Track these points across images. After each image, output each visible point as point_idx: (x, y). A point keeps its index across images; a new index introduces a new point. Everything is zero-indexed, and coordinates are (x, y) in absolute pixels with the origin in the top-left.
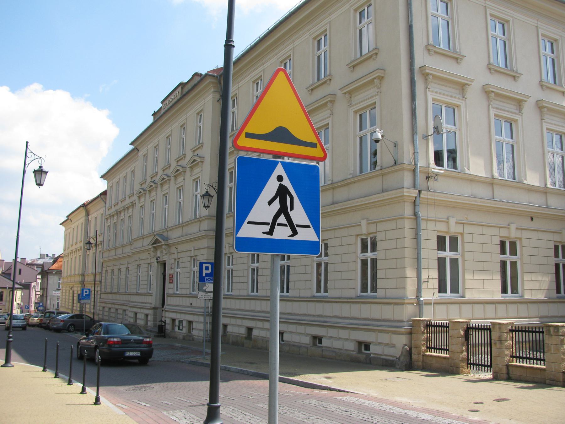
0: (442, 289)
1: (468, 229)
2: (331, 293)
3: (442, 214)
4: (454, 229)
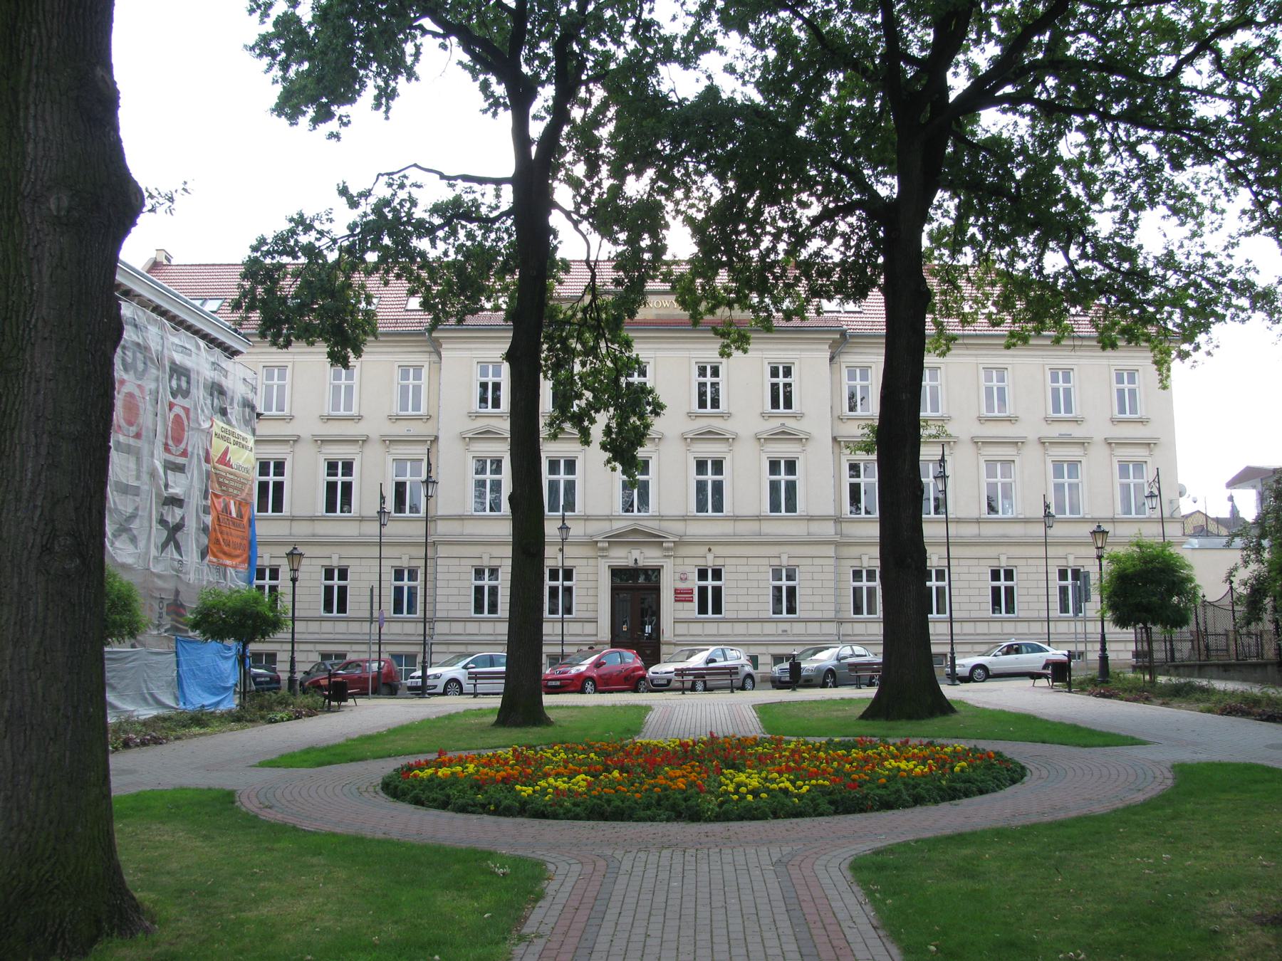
0: (858, 610)
1: (728, 561)
4: (1004, 563)
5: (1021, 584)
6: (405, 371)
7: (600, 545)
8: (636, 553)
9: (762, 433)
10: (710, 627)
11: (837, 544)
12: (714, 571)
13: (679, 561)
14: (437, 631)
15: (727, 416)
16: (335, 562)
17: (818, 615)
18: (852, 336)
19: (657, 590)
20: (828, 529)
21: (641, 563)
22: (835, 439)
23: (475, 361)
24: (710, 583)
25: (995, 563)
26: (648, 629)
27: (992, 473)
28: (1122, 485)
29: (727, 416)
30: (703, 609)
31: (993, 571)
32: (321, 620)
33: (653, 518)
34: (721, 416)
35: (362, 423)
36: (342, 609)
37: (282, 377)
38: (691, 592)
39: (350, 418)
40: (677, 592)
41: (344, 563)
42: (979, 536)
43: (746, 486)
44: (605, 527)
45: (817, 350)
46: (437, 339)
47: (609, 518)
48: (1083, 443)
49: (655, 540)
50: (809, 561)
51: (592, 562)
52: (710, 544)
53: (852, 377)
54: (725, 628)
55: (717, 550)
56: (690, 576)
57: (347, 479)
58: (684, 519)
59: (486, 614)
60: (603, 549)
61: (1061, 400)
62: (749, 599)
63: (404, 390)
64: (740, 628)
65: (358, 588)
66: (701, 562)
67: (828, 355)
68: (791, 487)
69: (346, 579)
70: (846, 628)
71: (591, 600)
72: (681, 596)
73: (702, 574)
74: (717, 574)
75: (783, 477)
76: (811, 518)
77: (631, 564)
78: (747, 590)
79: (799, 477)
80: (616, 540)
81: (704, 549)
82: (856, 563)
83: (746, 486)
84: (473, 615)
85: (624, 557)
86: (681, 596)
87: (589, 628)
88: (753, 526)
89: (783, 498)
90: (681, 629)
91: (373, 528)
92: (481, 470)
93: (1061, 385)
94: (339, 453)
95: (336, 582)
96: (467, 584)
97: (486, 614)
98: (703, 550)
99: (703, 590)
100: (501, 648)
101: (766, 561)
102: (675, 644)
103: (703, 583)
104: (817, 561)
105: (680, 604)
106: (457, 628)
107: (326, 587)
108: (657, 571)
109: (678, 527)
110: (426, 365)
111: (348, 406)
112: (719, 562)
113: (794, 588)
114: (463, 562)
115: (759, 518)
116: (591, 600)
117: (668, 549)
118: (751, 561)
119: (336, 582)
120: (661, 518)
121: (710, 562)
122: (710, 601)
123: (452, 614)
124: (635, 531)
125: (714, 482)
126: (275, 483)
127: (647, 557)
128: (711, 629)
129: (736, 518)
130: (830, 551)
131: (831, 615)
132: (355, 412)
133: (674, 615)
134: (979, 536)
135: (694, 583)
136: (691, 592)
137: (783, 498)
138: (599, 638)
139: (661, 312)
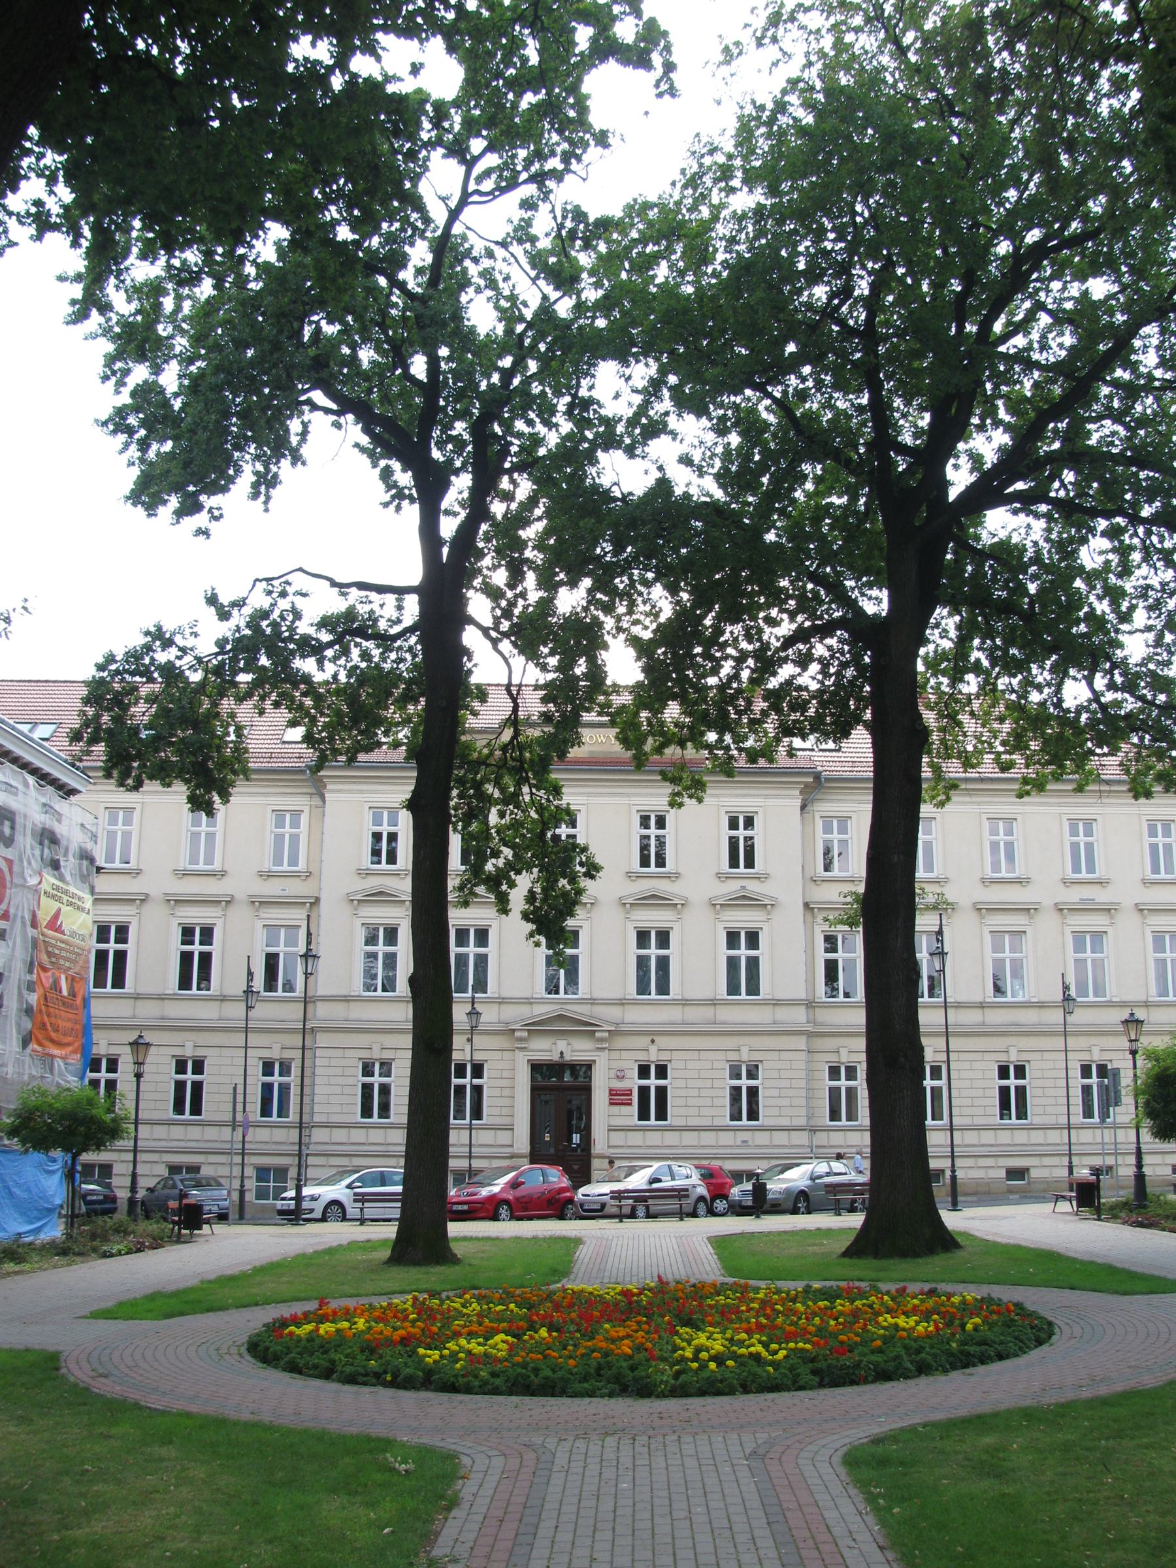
0: (835, 1115)
1: (676, 1055)
5: (1035, 1083)
6: (279, 815)
7: (517, 1034)
8: (562, 1045)
10: (653, 1137)
11: (810, 1035)
12: (657, 1067)
13: (615, 1055)
15: (675, 876)
16: (189, 1052)
17: (785, 1122)
18: (828, 780)
19: (586, 1090)
20: (798, 1017)
21: (568, 1057)
22: (806, 905)
23: (984, 817)
24: (653, 1082)
25: (1003, 1057)
26: (576, 1138)
27: (998, 948)
28: (1157, 960)
29: (675, 876)
30: (644, 1115)
33: (582, 1001)
35: (226, 880)
37: (128, 821)
38: (629, 1093)
39: (211, 874)
41: (200, 1052)
42: (984, 1024)
43: (698, 963)
44: (524, 1012)
47: (529, 1001)
48: (1108, 910)
49: (585, 1028)
51: (507, 1055)
52: (653, 1035)
53: (828, 829)
54: (671, 1138)
55: (662, 1041)
56: (628, 1074)
58: (622, 1002)
59: (275, 1118)
60: (521, 1039)
61: (1083, 857)
62: (701, 1102)
64: (690, 1138)
66: (642, 1056)
67: (798, 802)
68: (663, 963)
69: (665, 1078)
70: (821, 1138)
71: (506, 1102)
72: (618, 1098)
73: (644, 1072)
74: (662, 1072)
75: (653, 952)
76: (777, 1003)
77: (555, 1057)
78: (699, 1092)
80: (537, 1028)
82: (833, 1058)
83: (698, 963)
85: (548, 1049)
86: (618, 1098)
87: (503, 1137)
88: (706, 1013)
89: (744, 977)
90: (617, 1138)
91: (238, 1010)
92: (371, 940)
94: (197, 916)
96: (351, 1081)
97: (275, 1118)
99: (644, 1091)
101: (720, 1056)
104: (784, 1055)
106: (340, 1135)
107: (365, 1086)
108: (589, 1066)
109: (614, 1013)
110: (306, 809)
112: (664, 1056)
113: (1024, 1088)
114: (348, 1053)
115: (713, 1002)
116: (506, 1102)
117: (602, 1040)
118: (704, 1055)
120: (593, 1002)
121: (653, 1056)
122: (653, 1105)
124: (561, 1018)
127: (575, 1050)
128: (654, 1138)
129: (685, 1002)
130: (801, 1043)
131: (802, 1122)
132: (217, 866)
133: (608, 1123)
134: (984, 1024)
135: (634, 1082)
136: (629, 1093)
137: (744, 977)
138: (516, 1150)
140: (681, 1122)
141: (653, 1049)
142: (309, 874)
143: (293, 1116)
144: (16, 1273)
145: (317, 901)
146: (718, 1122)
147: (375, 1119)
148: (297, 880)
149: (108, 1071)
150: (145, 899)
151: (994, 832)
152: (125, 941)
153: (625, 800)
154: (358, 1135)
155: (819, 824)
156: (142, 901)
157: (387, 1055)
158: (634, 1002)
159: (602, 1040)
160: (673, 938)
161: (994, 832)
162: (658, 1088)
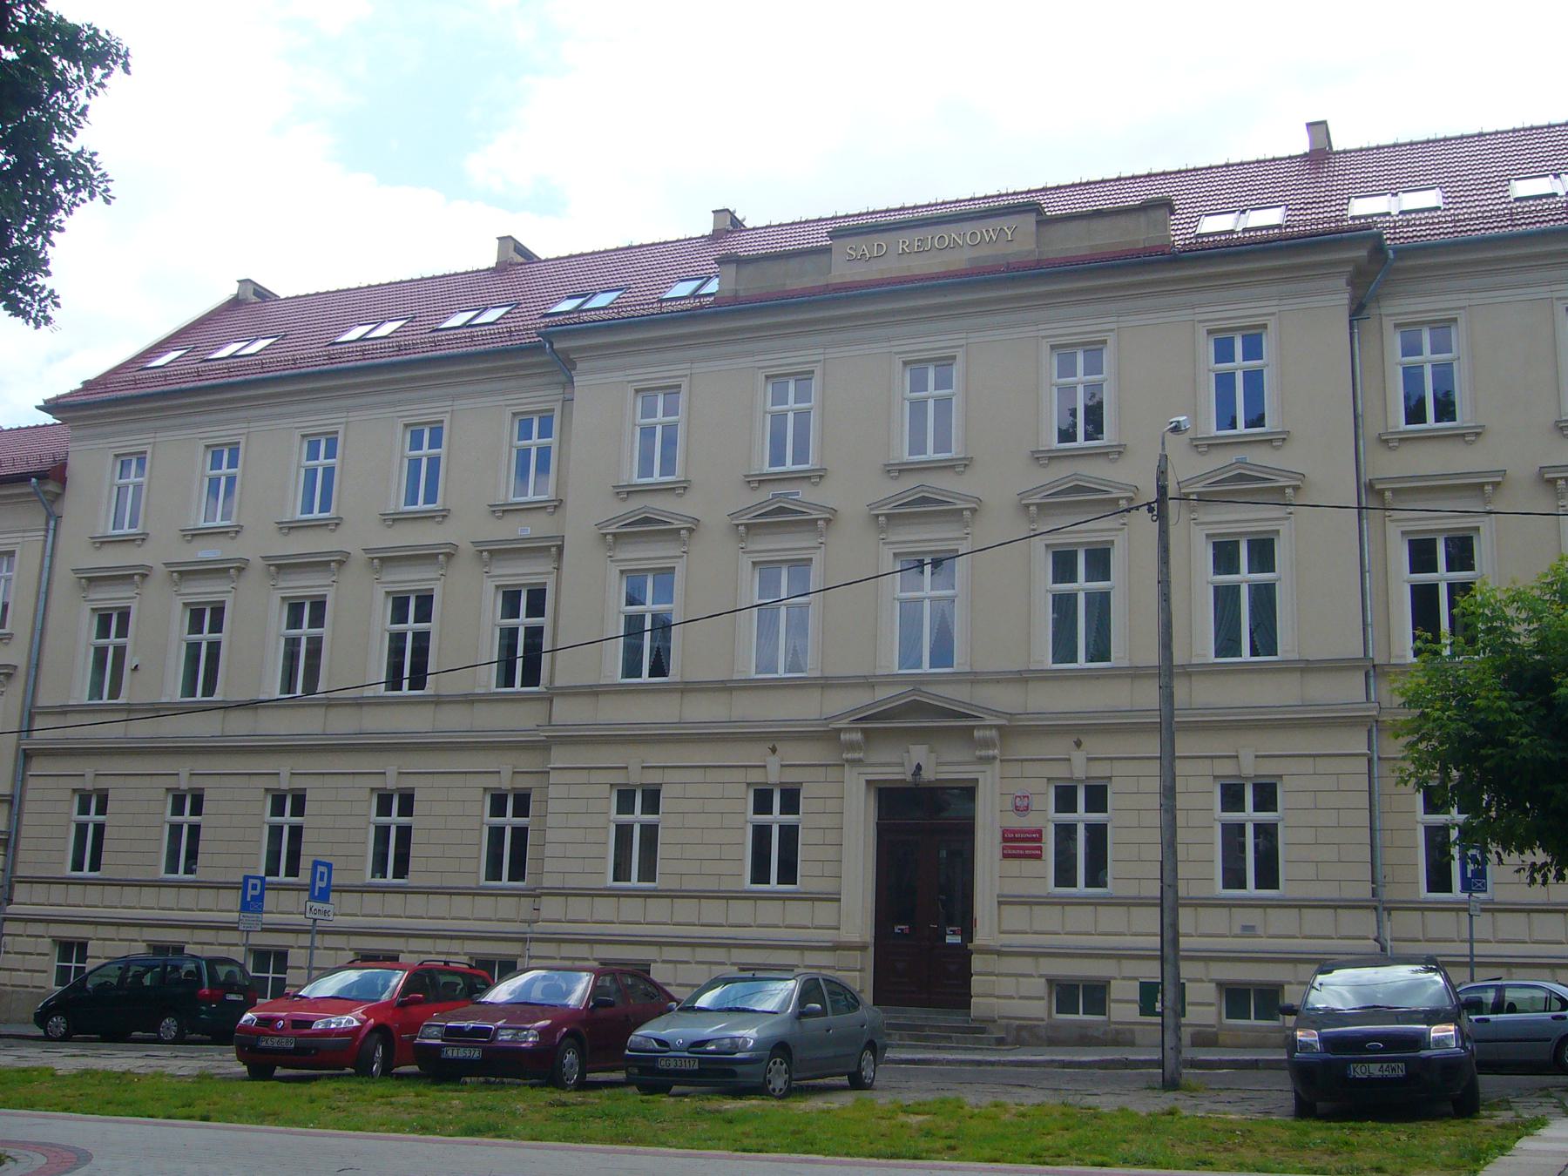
2: (201, 874)
3: (753, 754)
4: (1250, 768)
8: (918, 753)
9: (610, 522)
14: (544, 914)
19: (966, 831)
21: (928, 775)
24: (1081, 816)
29: (1276, 441)
30: (1065, 875)
31: (1226, 789)
32: (1423, 908)
34: (1103, 454)
36: (1096, 875)
38: (1037, 836)
40: (1009, 836)
45: (281, 416)
46: (566, 351)
47: (869, 682)
50: (1308, 766)
51: (833, 773)
52: (1077, 730)
56: (1035, 803)
57: (422, 626)
58: (1024, 678)
59: (634, 882)
60: (852, 746)
61: (1243, 404)
63: (1225, 383)
65: (1131, 825)
66: (1060, 771)
70: (1403, 924)
73: (1065, 799)
79: (1282, 575)
80: (881, 725)
81: (764, 748)
84: (483, 882)
86: (1020, 845)
87: (824, 912)
90: (1016, 917)
93: (1239, 365)
95: (776, 818)
98: (1059, 747)
99: (1065, 833)
100: (855, 958)
101: (739, 775)
102: (999, 953)
103: (1066, 817)
105: (1014, 866)
106: (579, 907)
107: (619, 828)
108: (968, 792)
111: (943, 443)
112: (1099, 770)
114: (597, 776)
119: (776, 818)
120: (974, 678)
121: (1080, 769)
123: (449, 881)
125: (310, 640)
126: (1089, 596)
127: (938, 764)
129: (1307, 667)
132: (956, 452)
135: (1046, 817)
139: (984, 251)
140: (434, 881)
141: (1078, 757)
142: (558, 505)
143: (304, 877)
144: (951, 1168)
145: (560, 549)
146: (1034, 889)
147: (773, 885)
148: (542, 516)
149: (97, 813)
150: (241, 567)
151: (1411, 348)
152: (428, 618)
153: (1542, 292)
154: (1048, 918)
155: (1395, 342)
156: (449, 556)
157: (652, 778)
158: (378, 702)
159: (987, 743)
160: (1282, 553)
161: (1411, 348)
162: (1090, 828)
